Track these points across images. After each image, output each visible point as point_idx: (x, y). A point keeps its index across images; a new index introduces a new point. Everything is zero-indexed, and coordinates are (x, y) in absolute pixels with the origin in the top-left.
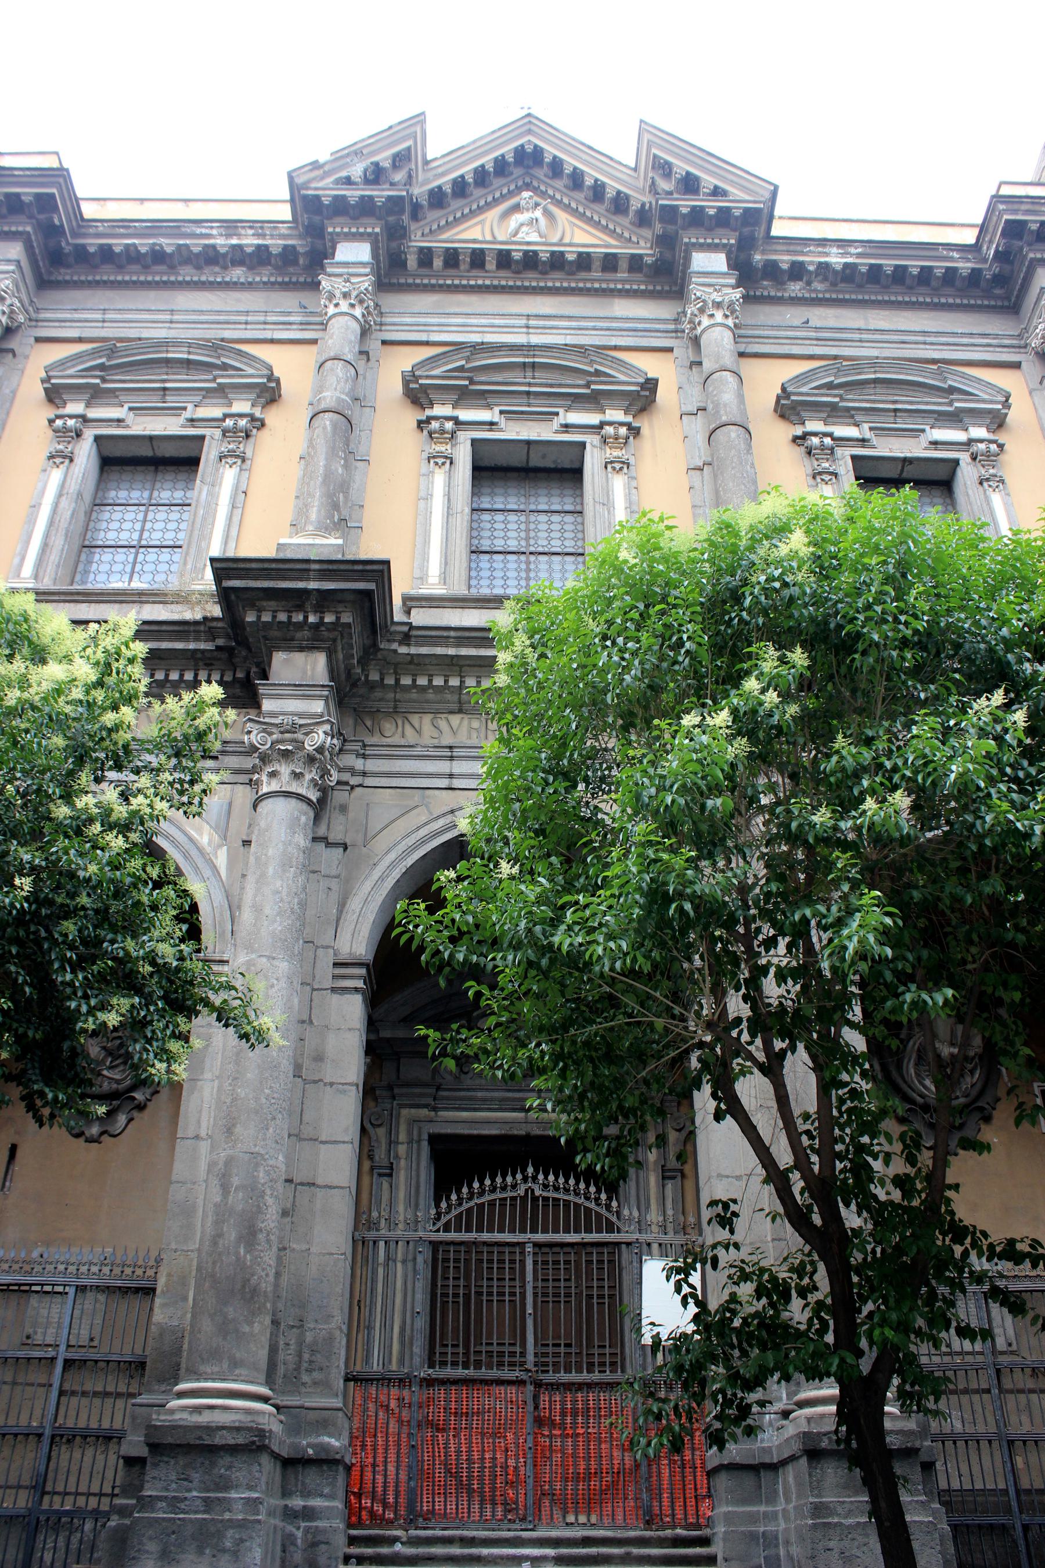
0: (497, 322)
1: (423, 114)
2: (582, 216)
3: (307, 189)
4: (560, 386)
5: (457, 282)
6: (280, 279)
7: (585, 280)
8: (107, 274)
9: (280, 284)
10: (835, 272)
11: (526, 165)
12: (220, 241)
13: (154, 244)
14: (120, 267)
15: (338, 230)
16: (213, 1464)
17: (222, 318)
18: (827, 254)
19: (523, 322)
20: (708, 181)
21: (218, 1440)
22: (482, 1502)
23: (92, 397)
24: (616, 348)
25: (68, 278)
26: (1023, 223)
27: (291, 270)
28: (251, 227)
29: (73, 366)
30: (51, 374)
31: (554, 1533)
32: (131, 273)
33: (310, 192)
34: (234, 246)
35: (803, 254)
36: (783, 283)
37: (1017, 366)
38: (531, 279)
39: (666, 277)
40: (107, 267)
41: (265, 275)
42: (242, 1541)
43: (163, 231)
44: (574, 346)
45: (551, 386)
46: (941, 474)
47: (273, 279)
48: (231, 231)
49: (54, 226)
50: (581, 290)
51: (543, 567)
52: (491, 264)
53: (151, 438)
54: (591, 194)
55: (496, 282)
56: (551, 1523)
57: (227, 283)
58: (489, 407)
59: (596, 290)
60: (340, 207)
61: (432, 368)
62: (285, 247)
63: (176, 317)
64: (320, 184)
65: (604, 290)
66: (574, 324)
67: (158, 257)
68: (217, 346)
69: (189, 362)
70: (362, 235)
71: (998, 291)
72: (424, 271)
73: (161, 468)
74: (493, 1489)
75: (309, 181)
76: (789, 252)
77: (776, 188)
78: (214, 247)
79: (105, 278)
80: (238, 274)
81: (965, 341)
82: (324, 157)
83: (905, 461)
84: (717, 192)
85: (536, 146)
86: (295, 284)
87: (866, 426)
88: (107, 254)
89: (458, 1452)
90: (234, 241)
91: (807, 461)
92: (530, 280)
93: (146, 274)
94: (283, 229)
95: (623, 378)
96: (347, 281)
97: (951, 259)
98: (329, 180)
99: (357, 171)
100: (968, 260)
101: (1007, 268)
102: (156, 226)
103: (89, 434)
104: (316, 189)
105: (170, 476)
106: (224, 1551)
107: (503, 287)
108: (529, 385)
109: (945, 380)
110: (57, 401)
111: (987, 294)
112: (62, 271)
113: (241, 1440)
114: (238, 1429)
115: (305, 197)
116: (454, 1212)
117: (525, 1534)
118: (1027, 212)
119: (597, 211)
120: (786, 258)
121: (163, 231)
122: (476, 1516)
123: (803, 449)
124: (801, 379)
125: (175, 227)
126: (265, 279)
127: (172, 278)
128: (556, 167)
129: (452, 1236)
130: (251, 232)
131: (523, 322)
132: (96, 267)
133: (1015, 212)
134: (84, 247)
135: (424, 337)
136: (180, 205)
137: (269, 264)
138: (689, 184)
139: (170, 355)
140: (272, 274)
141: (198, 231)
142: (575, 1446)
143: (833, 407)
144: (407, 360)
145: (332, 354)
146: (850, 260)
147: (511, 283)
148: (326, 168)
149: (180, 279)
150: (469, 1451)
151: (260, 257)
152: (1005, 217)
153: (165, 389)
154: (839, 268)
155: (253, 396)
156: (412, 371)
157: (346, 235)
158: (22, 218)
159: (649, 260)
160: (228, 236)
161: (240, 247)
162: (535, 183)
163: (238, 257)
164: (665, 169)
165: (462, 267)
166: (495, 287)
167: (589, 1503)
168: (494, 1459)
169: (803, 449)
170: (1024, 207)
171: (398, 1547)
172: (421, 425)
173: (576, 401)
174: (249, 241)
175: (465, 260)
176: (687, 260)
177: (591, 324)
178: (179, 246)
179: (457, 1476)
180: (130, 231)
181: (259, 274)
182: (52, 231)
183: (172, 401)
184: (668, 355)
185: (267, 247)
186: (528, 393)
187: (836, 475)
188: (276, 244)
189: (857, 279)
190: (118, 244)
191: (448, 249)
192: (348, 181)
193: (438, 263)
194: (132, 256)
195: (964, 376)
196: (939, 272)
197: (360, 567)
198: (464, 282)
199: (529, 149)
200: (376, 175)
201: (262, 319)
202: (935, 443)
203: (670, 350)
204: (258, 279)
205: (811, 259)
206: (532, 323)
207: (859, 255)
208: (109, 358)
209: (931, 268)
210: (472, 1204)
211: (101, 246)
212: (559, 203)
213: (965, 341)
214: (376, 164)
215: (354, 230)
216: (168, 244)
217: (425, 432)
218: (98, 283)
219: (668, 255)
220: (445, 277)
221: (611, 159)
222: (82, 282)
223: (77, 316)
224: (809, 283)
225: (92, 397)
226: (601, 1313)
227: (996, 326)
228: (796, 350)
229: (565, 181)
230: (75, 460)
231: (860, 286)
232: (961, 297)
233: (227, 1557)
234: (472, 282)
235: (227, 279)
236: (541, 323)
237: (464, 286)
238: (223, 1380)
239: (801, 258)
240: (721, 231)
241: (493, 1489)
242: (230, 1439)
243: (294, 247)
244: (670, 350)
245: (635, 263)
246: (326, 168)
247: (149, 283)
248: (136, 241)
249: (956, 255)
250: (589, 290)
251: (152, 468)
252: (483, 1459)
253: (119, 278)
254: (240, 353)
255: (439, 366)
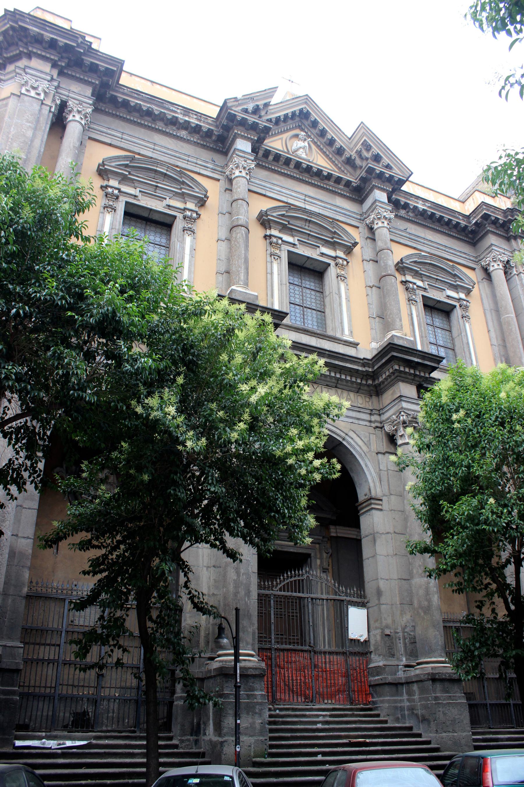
0: (293, 194)
1: (277, 87)
2: (321, 150)
3: (232, 110)
4: (322, 235)
5: (276, 169)
6: (202, 143)
7: (327, 184)
8: (122, 113)
9: (201, 144)
10: (419, 211)
11: (304, 119)
12: (180, 116)
13: (150, 107)
14: (130, 112)
15: (239, 132)
16: (247, 682)
17: (177, 155)
18: (418, 203)
19: (303, 197)
20: (386, 160)
21: (249, 673)
22: (297, 696)
23: (122, 180)
24: (338, 220)
25: (103, 109)
26: (490, 216)
27: (208, 139)
28: (196, 115)
29: (115, 162)
30: (105, 163)
31: (323, 706)
32: (134, 117)
33: (232, 112)
34: (186, 121)
35: (409, 200)
36: (399, 209)
37: (474, 269)
38: (306, 177)
39: (358, 193)
40: (123, 110)
41: (195, 138)
42: (262, 709)
43: (155, 102)
44: (322, 215)
45: (319, 234)
46: (447, 309)
47: (199, 141)
48: (186, 113)
49: (108, 84)
50: (324, 188)
51: (309, 314)
52: (292, 166)
53: (151, 210)
54: (328, 142)
55: (292, 174)
56: (319, 703)
57: (178, 136)
58: (293, 236)
59: (330, 190)
60: (243, 123)
61: (273, 212)
62: (209, 129)
63: (156, 148)
64: (236, 109)
65: (333, 191)
66: (323, 205)
67: (149, 113)
68: (182, 172)
69: (166, 174)
70: (249, 138)
71: (470, 236)
72: (264, 159)
73: (148, 223)
74: (301, 691)
75: (232, 106)
76: (405, 198)
77: (412, 173)
78: (177, 118)
79: (121, 115)
80: (183, 133)
81: (458, 254)
82: (239, 97)
83: (439, 302)
84: (388, 167)
85: (308, 111)
86: (208, 147)
87: (426, 283)
88: (125, 104)
89: (288, 677)
90: (187, 119)
91: (406, 293)
92: (306, 177)
93: (141, 119)
94: (210, 121)
95: (346, 239)
96: (245, 161)
97: (459, 219)
98: (240, 108)
99: (250, 107)
100: (464, 221)
101: (478, 229)
102: (152, 99)
103: (123, 200)
104: (235, 111)
105: (153, 229)
106: (256, 713)
107: (294, 177)
108: (310, 231)
109: (454, 270)
110: (104, 176)
111: (467, 236)
112: (101, 104)
113: (257, 673)
114: (256, 669)
115: (229, 113)
116: (283, 584)
117: (314, 707)
118: (492, 212)
119: (328, 150)
120: (403, 200)
121: (155, 102)
122: (295, 701)
123: (405, 287)
124: (409, 257)
125: (162, 102)
126: (195, 140)
127: (153, 126)
128: (315, 124)
129: (282, 593)
130: (195, 117)
131: (303, 197)
132: (118, 108)
133: (488, 210)
134: (116, 97)
135: (263, 192)
136: (149, 83)
137: (198, 133)
138: (377, 158)
139: (158, 169)
140: (198, 139)
141: (171, 108)
142: (326, 675)
143: (417, 272)
144: (265, 205)
145: (241, 197)
146: (425, 208)
147: (298, 176)
148: (240, 102)
149: (157, 127)
150: (292, 676)
151: (197, 129)
152: (485, 211)
153: (157, 186)
154: (421, 210)
155: (196, 202)
156: (266, 211)
157: (242, 136)
158: (95, 76)
159: (354, 185)
160: (184, 115)
161: (189, 122)
162: (303, 127)
163: (186, 126)
164: (368, 148)
165: (280, 163)
166: (291, 176)
167: (331, 696)
168: (301, 679)
169: (405, 287)
170: (491, 210)
171: (277, 711)
172: (265, 237)
173: (327, 243)
174: (194, 121)
175: (282, 160)
176: (371, 190)
177: (329, 207)
178: (161, 112)
179: (288, 686)
180: (139, 97)
181: (193, 137)
182: (105, 85)
183: (159, 193)
184: (356, 229)
185: (201, 126)
186: (309, 234)
187: (416, 301)
188: (205, 127)
189: (425, 216)
190: (133, 101)
191: (277, 153)
192: (246, 111)
193: (271, 158)
194: (137, 109)
195: (461, 271)
196: (454, 223)
197: (277, 313)
198: (279, 170)
199: (305, 111)
200: (256, 111)
201: (195, 161)
202: (448, 296)
203: (358, 227)
204: (192, 139)
205: (412, 203)
206: (307, 199)
207: (429, 207)
208: (131, 162)
209: (451, 220)
210: (288, 581)
211: (124, 99)
212: (315, 143)
213: (458, 254)
214: (258, 106)
215: (246, 135)
216: (156, 110)
217: (268, 241)
218: (117, 116)
219: (362, 185)
220: (272, 165)
221: (340, 130)
222: (110, 113)
223: (109, 132)
224: (408, 212)
225: (122, 180)
226: (293, 623)
227: (465, 249)
228: (402, 241)
229: (317, 131)
230: (117, 211)
231: (425, 219)
232: (458, 234)
233: (257, 715)
234: (283, 171)
235: (178, 134)
236: (310, 200)
237: (279, 172)
238: (245, 650)
239: (408, 202)
240: (387, 184)
241: (301, 691)
242: (253, 672)
243: (212, 130)
244: (358, 227)
245: (348, 184)
246: (240, 102)
247: (142, 124)
248: (142, 103)
249: (461, 218)
250: (327, 189)
251: (145, 222)
252: (297, 679)
253: (128, 117)
254: (193, 179)
255: (275, 212)
